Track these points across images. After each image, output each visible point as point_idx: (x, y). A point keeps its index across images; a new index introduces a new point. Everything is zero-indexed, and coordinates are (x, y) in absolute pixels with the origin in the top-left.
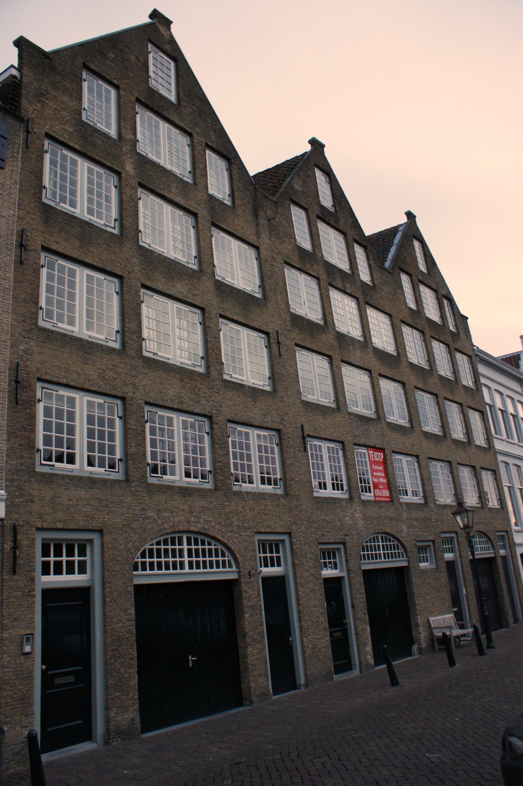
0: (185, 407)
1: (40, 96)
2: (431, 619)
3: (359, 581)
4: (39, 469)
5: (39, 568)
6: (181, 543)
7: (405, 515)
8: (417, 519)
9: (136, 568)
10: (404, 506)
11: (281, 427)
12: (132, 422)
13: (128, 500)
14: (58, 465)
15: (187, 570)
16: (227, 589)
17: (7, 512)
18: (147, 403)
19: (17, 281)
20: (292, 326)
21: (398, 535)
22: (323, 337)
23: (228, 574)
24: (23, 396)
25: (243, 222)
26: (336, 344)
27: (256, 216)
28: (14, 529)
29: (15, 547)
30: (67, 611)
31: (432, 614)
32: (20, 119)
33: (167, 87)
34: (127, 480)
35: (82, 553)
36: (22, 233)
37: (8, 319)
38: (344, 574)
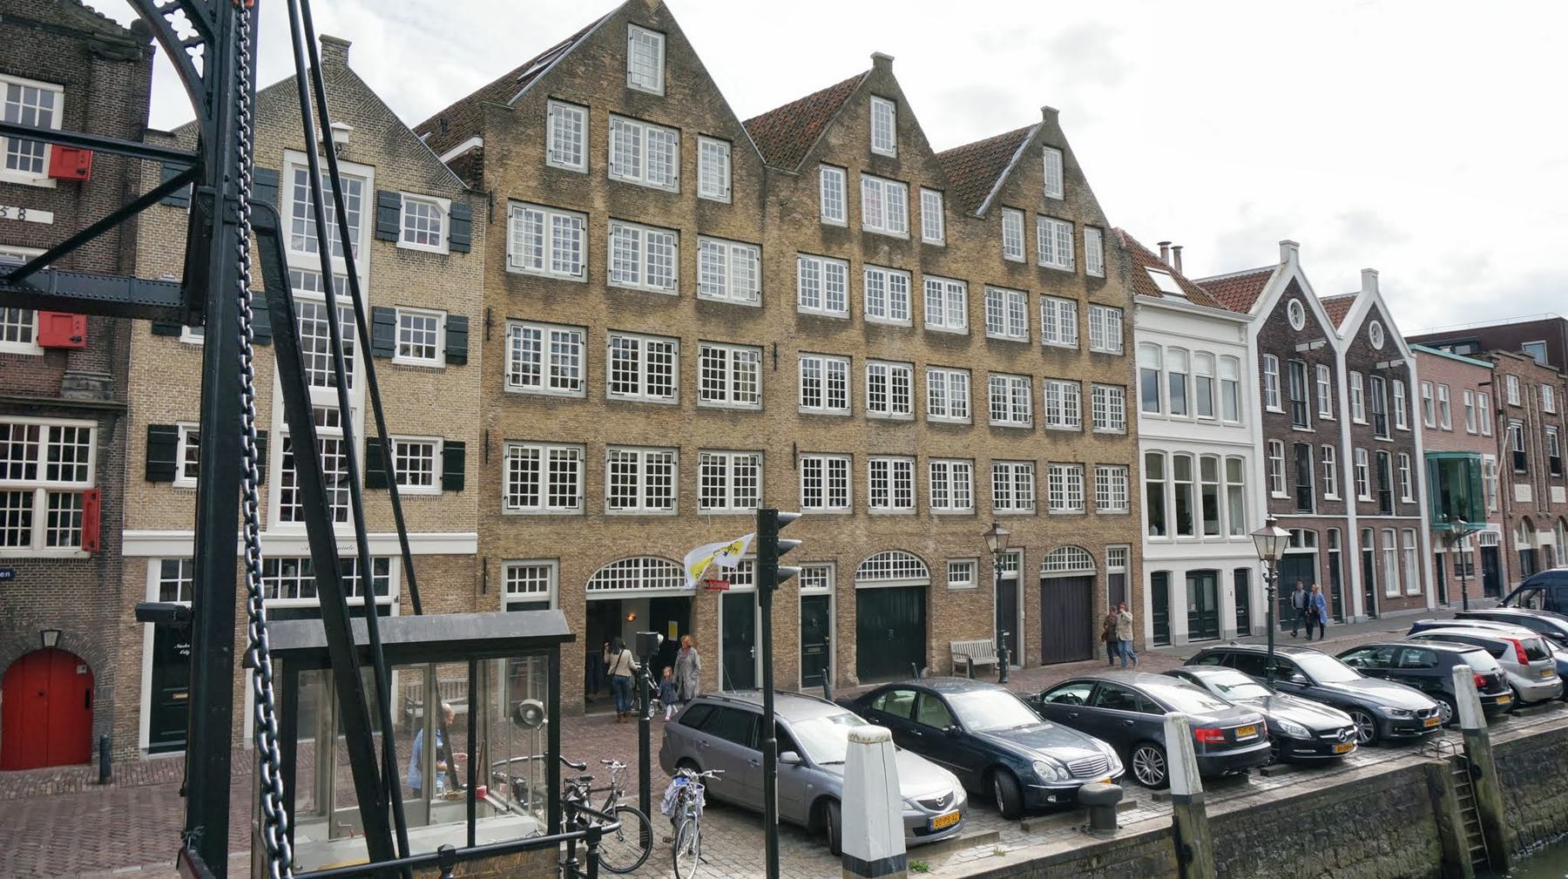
0: (650, 442)
1: (503, 159)
2: (953, 643)
3: (850, 602)
4: (506, 512)
5: (505, 587)
6: (637, 565)
7: (934, 530)
8: (953, 534)
9: (591, 586)
10: (936, 520)
11: (767, 447)
12: (593, 464)
13: (585, 531)
14: (523, 507)
15: (641, 587)
16: (1089, 581)
17: (480, 549)
18: (609, 444)
19: (484, 357)
20: (798, 331)
21: (919, 552)
22: (1029, 356)
23: (1090, 572)
24: (491, 456)
25: (741, 221)
26: (862, 340)
27: (763, 206)
28: (485, 562)
29: (485, 574)
30: (1008, 590)
31: (956, 637)
32: (484, 195)
33: (884, 143)
34: (918, 515)
35: (543, 574)
36: (489, 312)
37: (478, 392)
38: (832, 593)
